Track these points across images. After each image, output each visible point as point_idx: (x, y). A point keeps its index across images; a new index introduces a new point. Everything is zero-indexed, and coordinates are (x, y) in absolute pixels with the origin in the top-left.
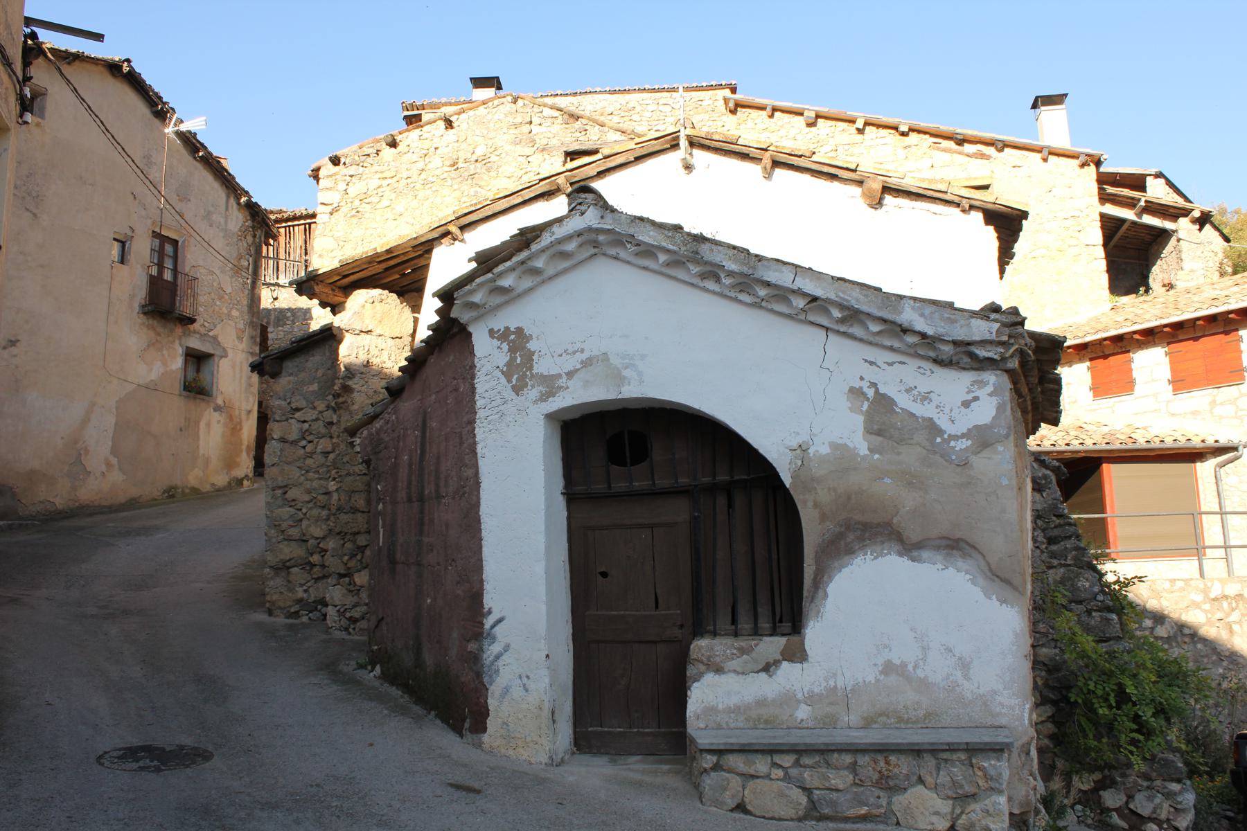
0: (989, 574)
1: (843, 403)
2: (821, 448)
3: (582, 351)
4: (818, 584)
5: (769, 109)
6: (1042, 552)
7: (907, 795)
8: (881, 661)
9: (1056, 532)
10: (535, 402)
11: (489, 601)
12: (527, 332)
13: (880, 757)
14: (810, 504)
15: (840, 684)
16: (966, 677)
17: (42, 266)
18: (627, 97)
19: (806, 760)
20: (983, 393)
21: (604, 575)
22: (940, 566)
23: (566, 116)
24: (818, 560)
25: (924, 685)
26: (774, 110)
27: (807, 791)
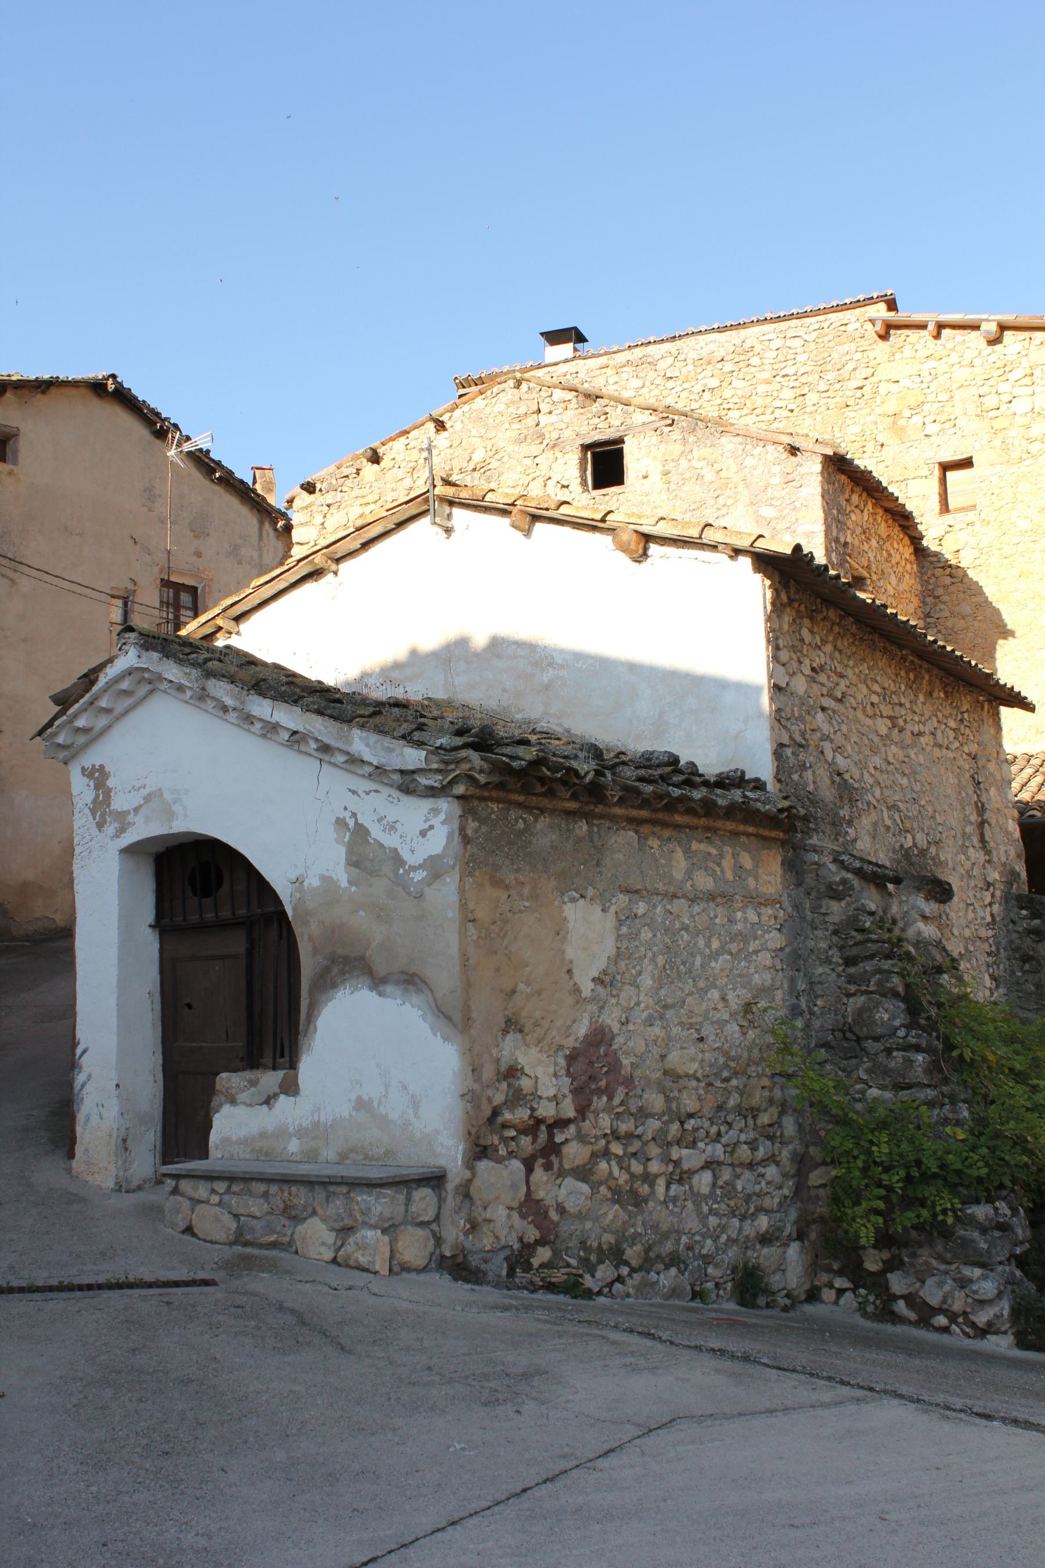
0: (436, 1011)
1: (329, 833)
2: (313, 882)
3: (144, 787)
4: (311, 1018)
5: (931, 327)
6: (839, 976)
7: (306, 1225)
8: (354, 1097)
9: (854, 951)
10: (112, 838)
11: (80, 1034)
12: (107, 769)
13: (285, 1187)
14: (306, 938)
15: (323, 1119)
16: (417, 1116)
17: (23, 641)
18: (743, 333)
19: (235, 1188)
20: (436, 821)
21: (189, 1006)
22: (399, 1001)
23: (581, 398)
24: (311, 993)
25: (384, 1122)
26: (941, 326)
27: (236, 1216)
